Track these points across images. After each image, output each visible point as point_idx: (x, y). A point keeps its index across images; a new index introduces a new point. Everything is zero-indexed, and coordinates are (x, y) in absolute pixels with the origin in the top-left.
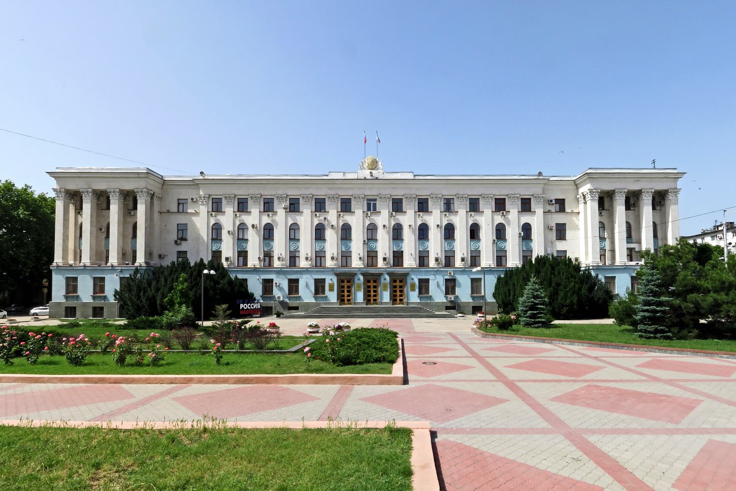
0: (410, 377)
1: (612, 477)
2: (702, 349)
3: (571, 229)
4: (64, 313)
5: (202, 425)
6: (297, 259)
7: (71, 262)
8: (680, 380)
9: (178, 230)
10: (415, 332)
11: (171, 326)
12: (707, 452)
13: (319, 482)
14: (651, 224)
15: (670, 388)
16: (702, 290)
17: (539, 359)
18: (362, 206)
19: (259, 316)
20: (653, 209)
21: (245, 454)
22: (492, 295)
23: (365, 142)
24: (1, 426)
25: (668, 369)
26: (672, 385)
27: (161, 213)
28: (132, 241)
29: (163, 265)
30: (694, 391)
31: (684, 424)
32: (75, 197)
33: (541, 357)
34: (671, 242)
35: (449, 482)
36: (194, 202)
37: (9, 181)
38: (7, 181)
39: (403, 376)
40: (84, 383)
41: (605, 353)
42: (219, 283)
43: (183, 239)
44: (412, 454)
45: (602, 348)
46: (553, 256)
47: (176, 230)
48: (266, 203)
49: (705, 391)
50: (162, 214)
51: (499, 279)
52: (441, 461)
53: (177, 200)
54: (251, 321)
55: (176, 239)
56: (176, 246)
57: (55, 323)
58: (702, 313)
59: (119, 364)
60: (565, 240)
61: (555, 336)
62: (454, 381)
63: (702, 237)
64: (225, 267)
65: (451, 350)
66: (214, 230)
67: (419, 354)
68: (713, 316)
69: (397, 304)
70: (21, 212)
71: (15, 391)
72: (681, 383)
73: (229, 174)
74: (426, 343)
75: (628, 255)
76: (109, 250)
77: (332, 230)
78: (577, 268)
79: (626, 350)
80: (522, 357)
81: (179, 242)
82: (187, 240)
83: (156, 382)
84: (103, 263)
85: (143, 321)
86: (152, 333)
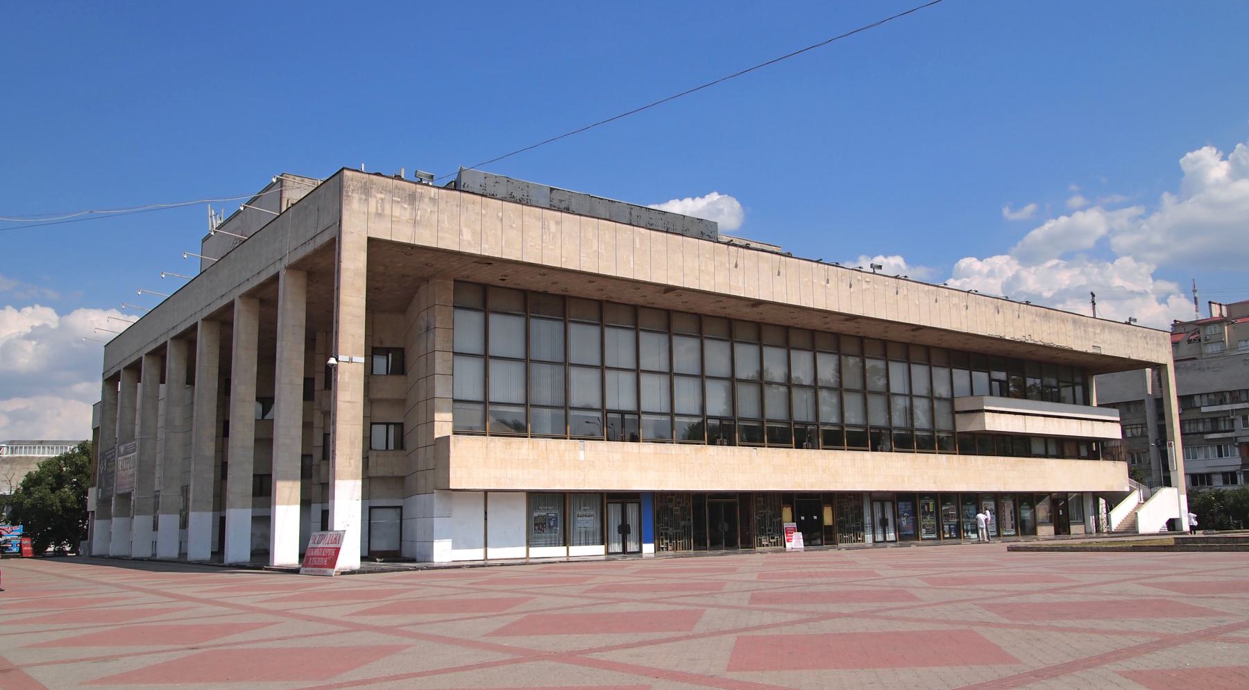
2: (100, 574)
3: (231, 507)
4: (212, 475)
5: (373, 202)
7: (380, 212)
8: (591, 650)
12: (752, 594)
15: (1220, 647)
17: (551, 315)
18: (413, 520)
20: (304, 400)
21: (34, 540)
22: (682, 202)
26: (584, 663)
30: (501, 649)
31: (699, 628)
33: (151, 622)
34: (795, 525)
44: (827, 379)
46: (1217, 153)
48: (623, 418)
49: (359, 678)
52: (585, 363)
54: (535, 598)
60: (19, 311)
61: (79, 470)
63: (153, 558)
65: (470, 584)
67: (539, 313)
70: (671, 531)
71: (801, 386)
72: (595, 656)
74: (21, 601)
76: (228, 422)
78: (729, 195)
85: (381, 206)
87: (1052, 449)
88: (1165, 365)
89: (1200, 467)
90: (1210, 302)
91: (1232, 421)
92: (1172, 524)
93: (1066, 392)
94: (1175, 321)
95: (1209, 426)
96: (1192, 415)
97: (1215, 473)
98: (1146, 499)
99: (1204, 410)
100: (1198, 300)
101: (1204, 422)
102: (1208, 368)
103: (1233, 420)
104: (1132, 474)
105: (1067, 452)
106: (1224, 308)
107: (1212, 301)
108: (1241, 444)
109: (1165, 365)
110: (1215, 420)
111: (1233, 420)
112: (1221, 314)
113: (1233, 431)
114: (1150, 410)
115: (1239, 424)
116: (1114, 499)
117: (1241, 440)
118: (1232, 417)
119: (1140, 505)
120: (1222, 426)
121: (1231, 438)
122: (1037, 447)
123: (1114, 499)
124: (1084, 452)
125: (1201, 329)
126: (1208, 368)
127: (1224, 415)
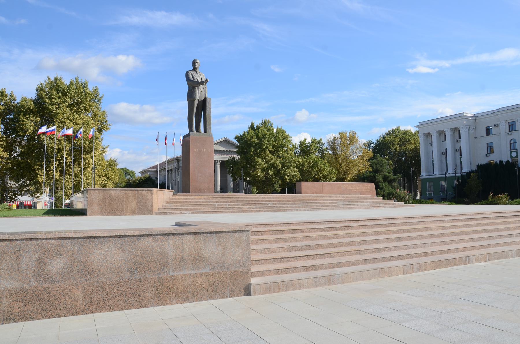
0: (514, 118)
1: (310, 134)
6: (476, 115)
9: (487, 147)
10: (81, 192)
11: (234, 299)
19: (324, 265)
24: (519, 198)
25: (420, 156)
27: (476, 138)
28: (253, 296)
29: (34, 98)
35: (225, 229)
36: (510, 135)
38: (71, 80)
40: (290, 200)
41: (440, 218)
43: (492, 152)
45: (517, 218)
47: (486, 147)
48: (511, 125)
52: (354, 220)
53: (486, 144)
55: (486, 153)
56: (508, 136)
58: (304, 110)
62: (183, 234)
66: (488, 148)
68: (7, 158)
73: (499, 115)
79: (485, 220)
80: (130, 190)
81: (488, 155)
82: (493, 153)
86: (36, 187)
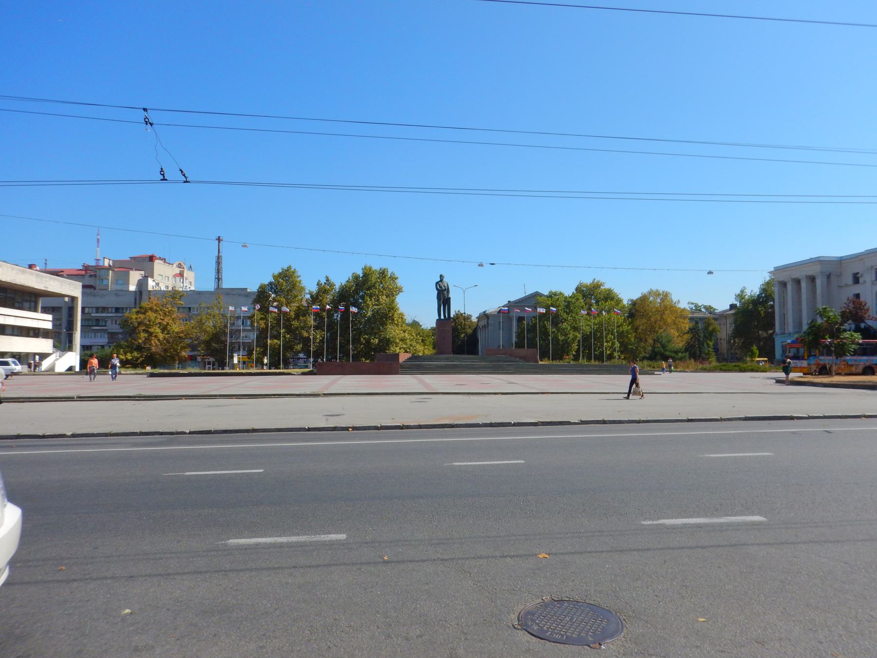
13: (584, 312)
14: (185, 183)
16: (100, 310)
23: (491, 264)
32: (784, 284)
37: (563, 360)
39: (224, 287)
42: (658, 342)
50: (353, 254)
51: (775, 358)
52: (74, 102)
57: (828, 368)
59: (254, 300)
62: (221, 406)
64: (259, 307)
69: (175, 369)
75: (216, 262)
77: (867, 302)
83: (847, 371)
84: (547, 559)
87: (31, 333)
88: (77, 298)
89: (88, 342)
90: (104, 258)
91: (106, 321)
92: (71, 369)
93: (26, 305)
94: (84, 264)
95: (94, 323)
96: (88, 317)
97: (95, 346)
98: (60, 357)
99: (93, 315)
100: (100, 241)
101: (92, 321)
102: (98, 295)
103: (106, 321)
104: (54, 346)
105: (15, 333)
106: (111, 261)
107: (105, 257)
108: (108, 332)
109: (77, 298)
110: (97, 320)
111: (106, 321)
112: (109, 264)
113: (105, 326)
114: (65, 312)
115: (109, 323)
116: (44, 356)
117: (109, 331)
118: (106, 320)
119: (57, 360)
120: (101, 323)
121: (103, 330)
122: (8, 331)
123: (44, 356)
124: (31, 334)
125: (98, 271)
126: (98, 295)
127: (103, 318)
